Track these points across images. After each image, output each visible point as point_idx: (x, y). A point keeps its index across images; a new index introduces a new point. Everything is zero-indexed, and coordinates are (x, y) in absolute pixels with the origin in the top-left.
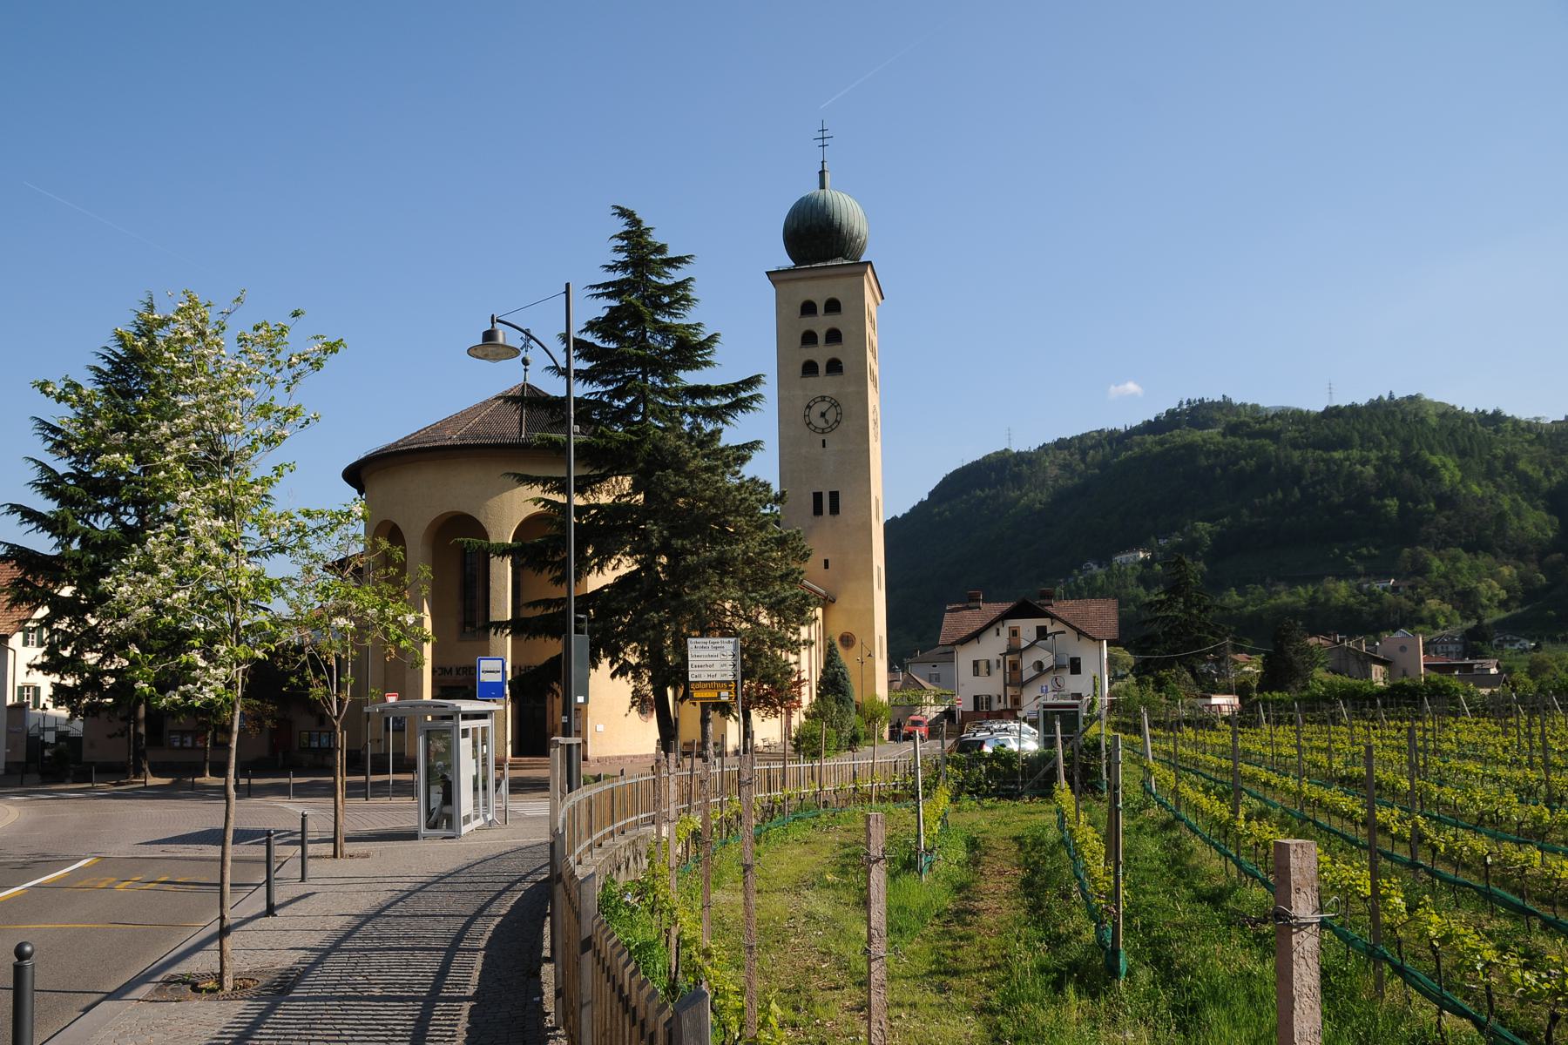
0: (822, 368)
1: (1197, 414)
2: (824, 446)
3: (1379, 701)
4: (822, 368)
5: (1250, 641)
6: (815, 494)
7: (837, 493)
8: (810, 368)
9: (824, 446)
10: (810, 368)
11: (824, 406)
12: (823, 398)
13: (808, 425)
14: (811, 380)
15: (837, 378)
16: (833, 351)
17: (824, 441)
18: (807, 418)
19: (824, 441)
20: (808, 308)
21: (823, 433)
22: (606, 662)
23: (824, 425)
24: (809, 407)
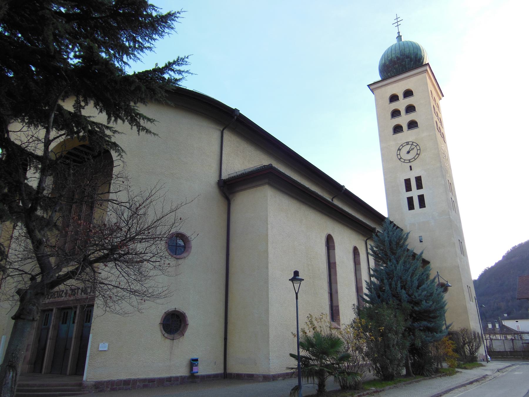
0: (405, 127)
1: (514, 248)
2: (411, 169)
3: (78, 36)
4: (405, 127)
5: (51, 47)
6: (422, 188)
7: (420, 207)
8: (398, 129)
9: (411, 169)
10: (398, 129)
11: (408, 148)
12: (408, 143)
13: (400, 159)
14: (399, 135)
15: (414, 131)
16: (412, 116)
17: (411, 167)
18: (399, 156)
19: (411, 167)
20: (394, 98)
21: (410, 162)
22: (373, 234)
23: (415, 149)
24: (399, 150)
